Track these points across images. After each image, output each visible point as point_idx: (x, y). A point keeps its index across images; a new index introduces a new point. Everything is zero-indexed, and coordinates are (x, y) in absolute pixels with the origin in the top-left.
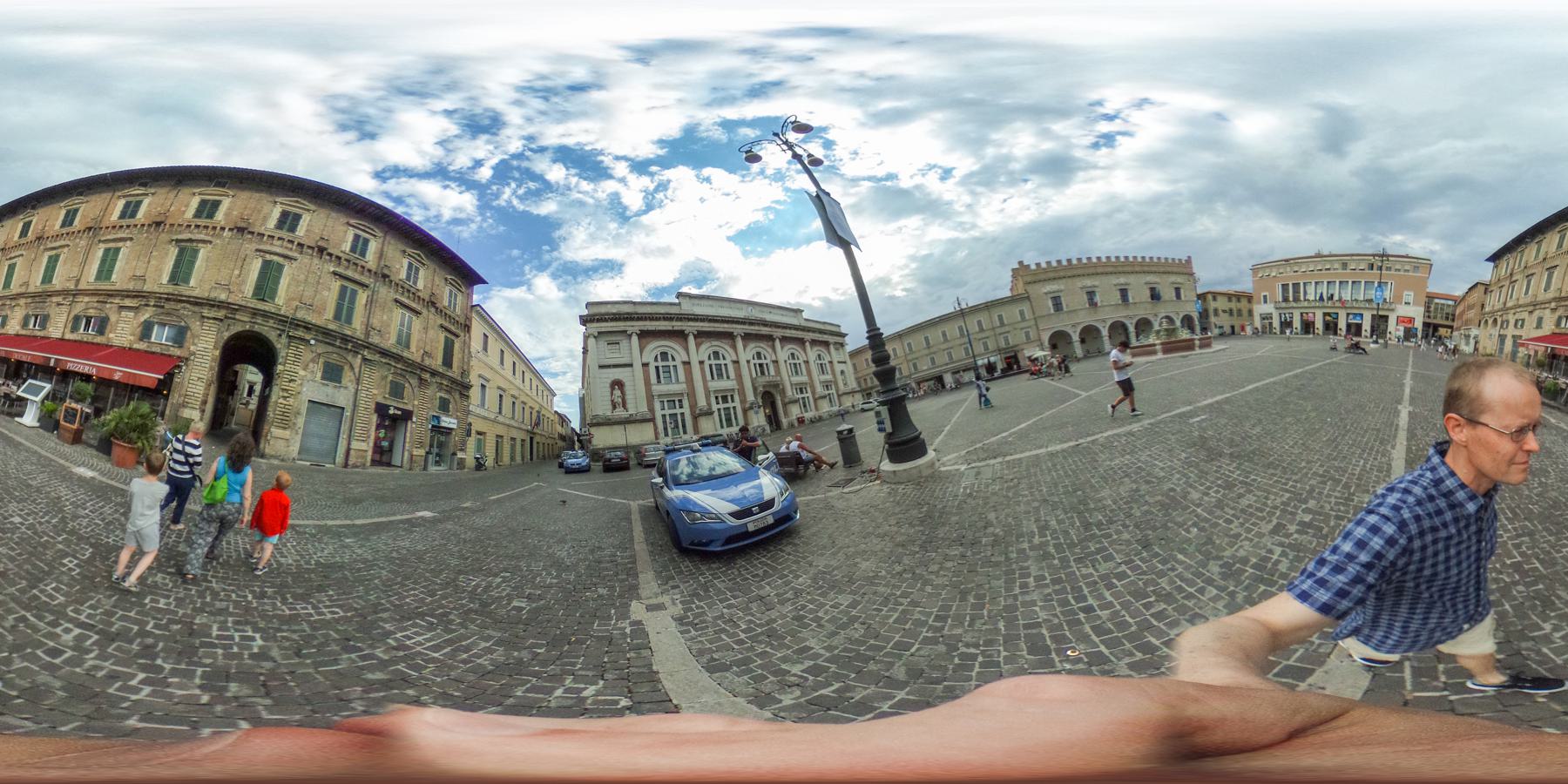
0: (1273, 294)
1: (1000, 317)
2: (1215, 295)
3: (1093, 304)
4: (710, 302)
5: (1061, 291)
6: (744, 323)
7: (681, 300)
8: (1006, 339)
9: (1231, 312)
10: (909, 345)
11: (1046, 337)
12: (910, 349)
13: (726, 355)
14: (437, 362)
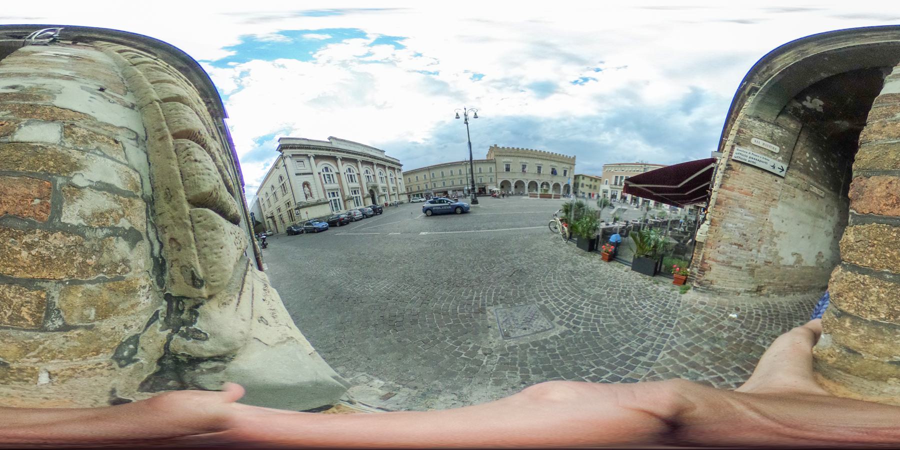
0: (610, 181)
1: (480, 169)
2: (584, 177)
3: (524, 171)
4: (346, 143)
5: (511, 162)
6: (361, 155)
7: (331, 140)
8: (481, 180)
9: (590, 186)
10: (433, 174)
11: (499, 182)
12: (433, 176)
13: (354, 171)
14: (425, 189)
